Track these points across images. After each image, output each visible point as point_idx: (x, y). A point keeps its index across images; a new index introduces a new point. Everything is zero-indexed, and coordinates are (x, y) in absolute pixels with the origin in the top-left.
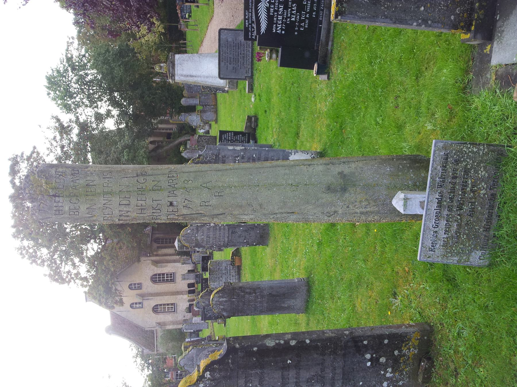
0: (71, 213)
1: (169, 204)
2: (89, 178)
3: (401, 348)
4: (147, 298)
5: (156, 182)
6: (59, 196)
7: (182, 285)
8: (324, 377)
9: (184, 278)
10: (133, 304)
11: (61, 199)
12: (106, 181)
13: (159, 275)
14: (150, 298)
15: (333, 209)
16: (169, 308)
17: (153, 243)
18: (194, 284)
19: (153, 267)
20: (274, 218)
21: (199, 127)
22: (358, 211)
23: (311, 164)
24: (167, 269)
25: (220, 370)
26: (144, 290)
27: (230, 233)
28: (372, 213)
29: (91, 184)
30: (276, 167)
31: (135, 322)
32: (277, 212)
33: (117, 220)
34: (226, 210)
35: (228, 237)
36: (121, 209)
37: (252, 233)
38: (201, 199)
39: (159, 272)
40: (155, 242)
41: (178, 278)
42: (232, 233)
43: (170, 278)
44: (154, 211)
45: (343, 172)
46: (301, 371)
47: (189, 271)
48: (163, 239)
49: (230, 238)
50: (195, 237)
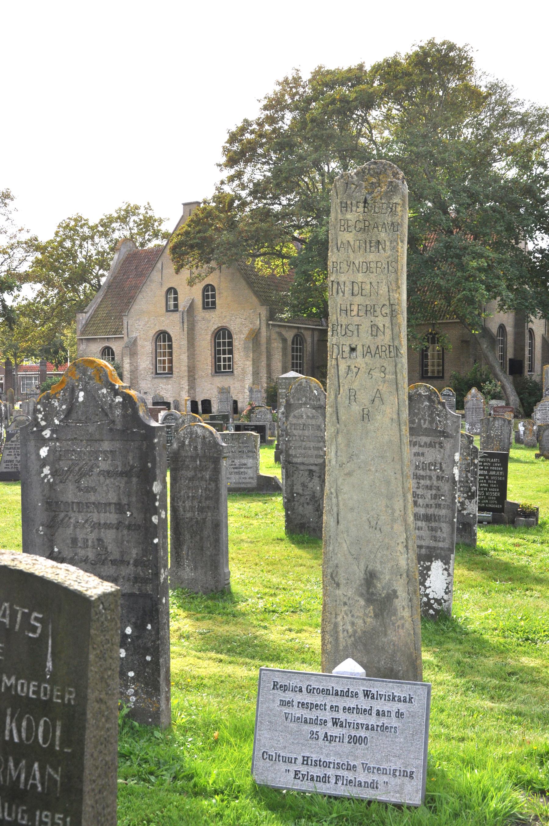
0: (343, 222)
1: (353, 346)
2: (388, 243)
3: (138, 681)
4: (185, 320)
5: (382, 329)
6: (365, 207)
7: (209, 388)
8: (103, 564)
9: (224, 391)
10: (176, 293)
11: (361, 209)
12: (384, 265)
13: (230, 344)
14: (185, 326)
15: (343, 581)
16: (164, 363)
17: (295, 331)
18: (210, 411)
19: (246, 331)
20: (331, 493)
21: (529, 423)
22: (339, 618)
23: (407, 549)
24: (242, 360)
25: (124, 416)
26: (200, 313)
27: (313, 468)
28: (337, 639)
29: (380, 246)
30: (404, 496)
31: (140, 296)
32: (340, 498)
33: (332, 279)
34: (343, 426)
35: (303, 464)
36: (347, 283)
37: (309, 509)
38: (359, 390)
39: (236, 343)
40: (296, 336)
41: (221, 381)
42: (311, 471)
43: (222, 366)
44: (344, 327)
45: (397, 597)
46: (115, 530)
47: (235, 402)
48: (301, 350)
49: (302, 467)
50: (305, 404)
